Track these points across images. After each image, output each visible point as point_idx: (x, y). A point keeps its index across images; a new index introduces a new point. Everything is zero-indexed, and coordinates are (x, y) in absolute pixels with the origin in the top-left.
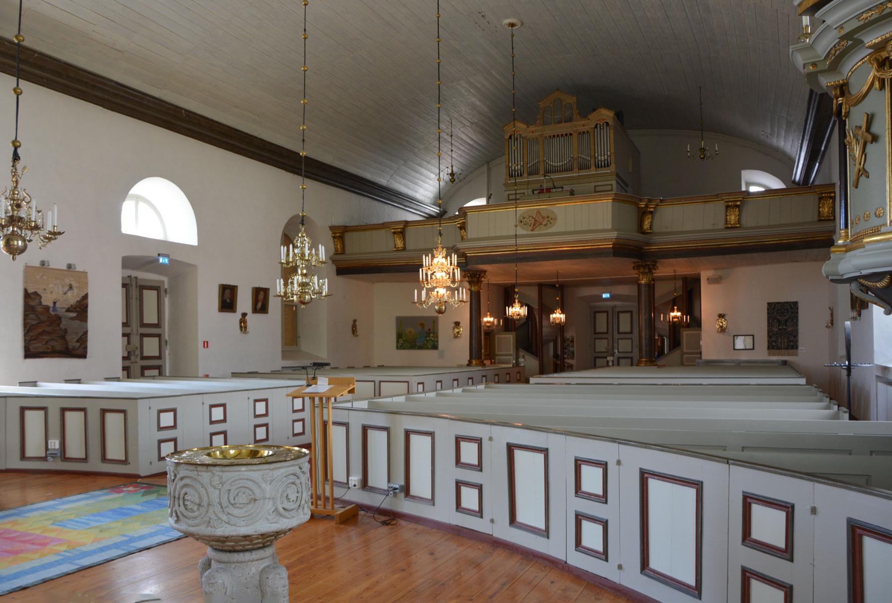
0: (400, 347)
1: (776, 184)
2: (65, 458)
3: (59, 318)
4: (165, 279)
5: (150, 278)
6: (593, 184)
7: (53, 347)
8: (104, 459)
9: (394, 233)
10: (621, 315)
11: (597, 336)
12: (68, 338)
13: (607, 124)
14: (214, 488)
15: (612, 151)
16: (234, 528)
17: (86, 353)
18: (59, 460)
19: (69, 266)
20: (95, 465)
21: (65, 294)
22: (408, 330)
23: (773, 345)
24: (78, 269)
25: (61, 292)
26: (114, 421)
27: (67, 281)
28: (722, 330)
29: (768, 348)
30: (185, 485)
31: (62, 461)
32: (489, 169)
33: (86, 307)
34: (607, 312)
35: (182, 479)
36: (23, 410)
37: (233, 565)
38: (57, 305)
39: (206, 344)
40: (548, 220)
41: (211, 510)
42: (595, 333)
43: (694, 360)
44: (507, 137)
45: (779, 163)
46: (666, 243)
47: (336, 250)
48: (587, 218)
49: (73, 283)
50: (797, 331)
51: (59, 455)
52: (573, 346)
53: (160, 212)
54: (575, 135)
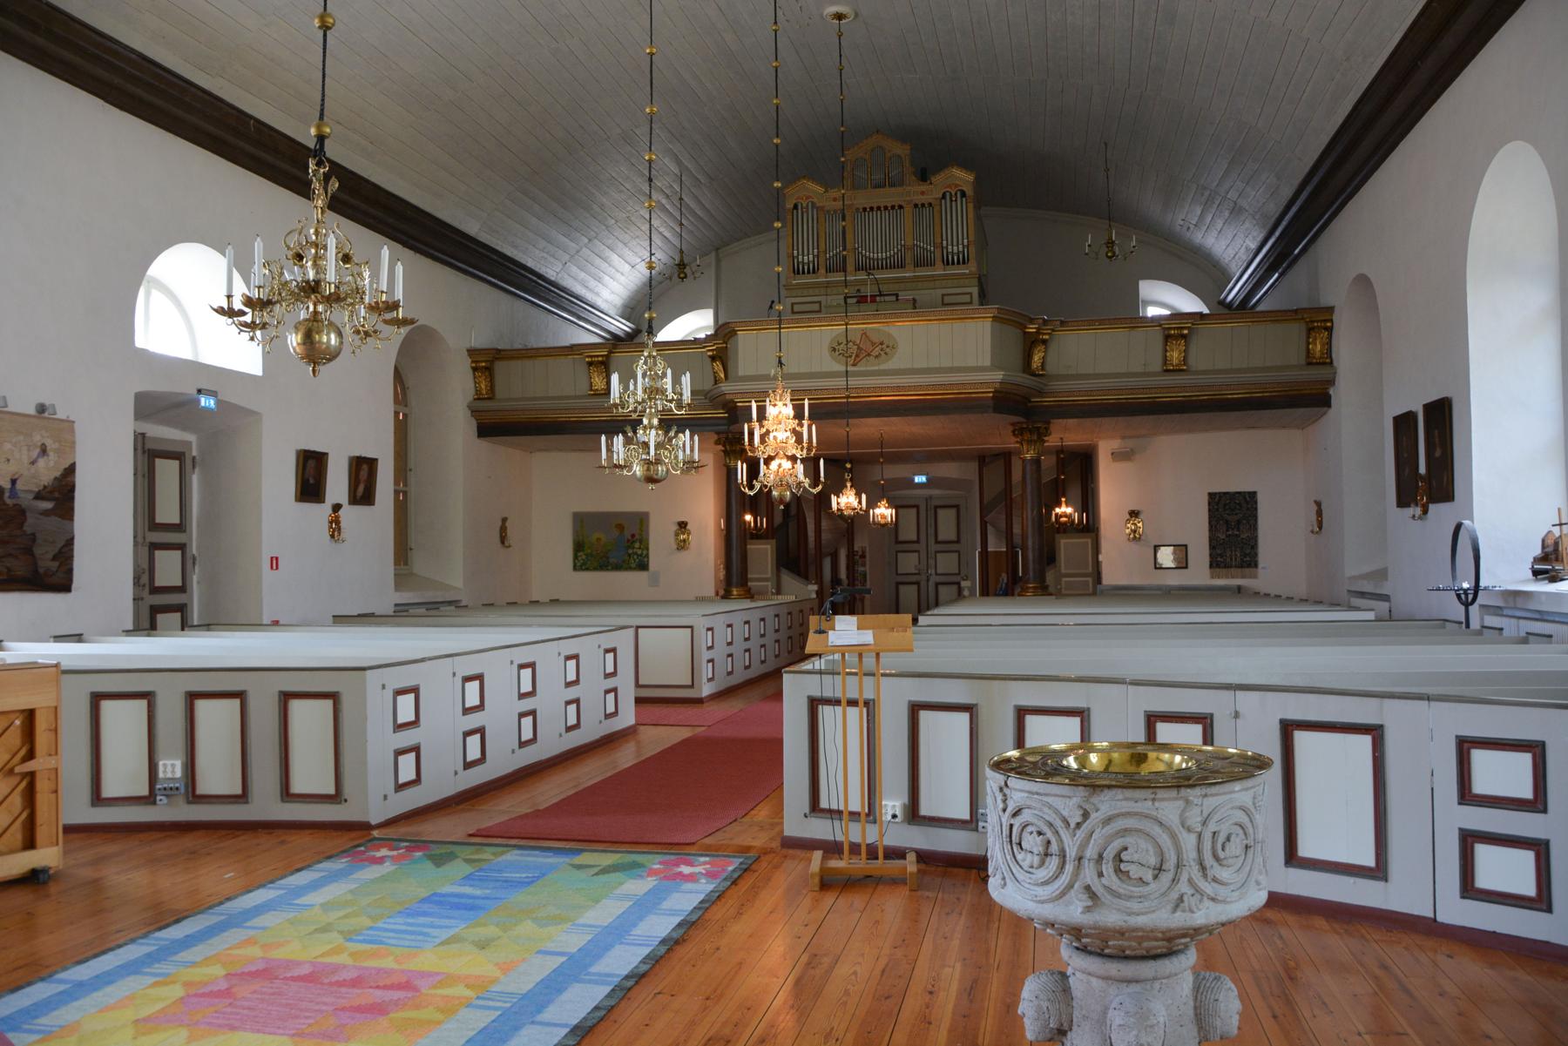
0: (579, 566)
1: (1189, 303)
2: (195, 798)
3: (21, 512)
4: (191, 438)
5: (181, 430)
6: (940, 292)
7: (9, 570)
8: (287, 794)
9: (590, 364)
10: (941, 512)
11: (900, 547)
12: (38, 551)
13: (963, 194)
14: (1189, 830)
15: (972, 238)
16: (1220, 907)
17: (71, 580)
18: (181, 800)
19: (41, 409)
20: (266, 806)
21: (33, 463)
22: (596, 535)
23: (1217, 562)
24: (61, 415)
25: (26, 460)
26: (309, 719)
27: (37, 438)
28: (1136, 537)
29: (1211, 566)
30: (1125, 832)
31: (189, 802)
32: (718, 261)
33: (72, 489)
34: (917, 507)
35: (1108, 821)
36: (97, 698)
37: (1157, 985)
38: (19, 486)
39: (275, 562)
40: (885, 348)
41: (1184, 877)
42: (897, 542)
43: (1092, 586)
44: (790, 206)
45: (1197, 269)
46: (1071, 393)
47: (478, 391)
48: (948, 348)
49: (49, 443)
50: (1255, 539)
51: (182, 790)
52: (864, 565)
53: (190, 309)
54: (908, 209)
